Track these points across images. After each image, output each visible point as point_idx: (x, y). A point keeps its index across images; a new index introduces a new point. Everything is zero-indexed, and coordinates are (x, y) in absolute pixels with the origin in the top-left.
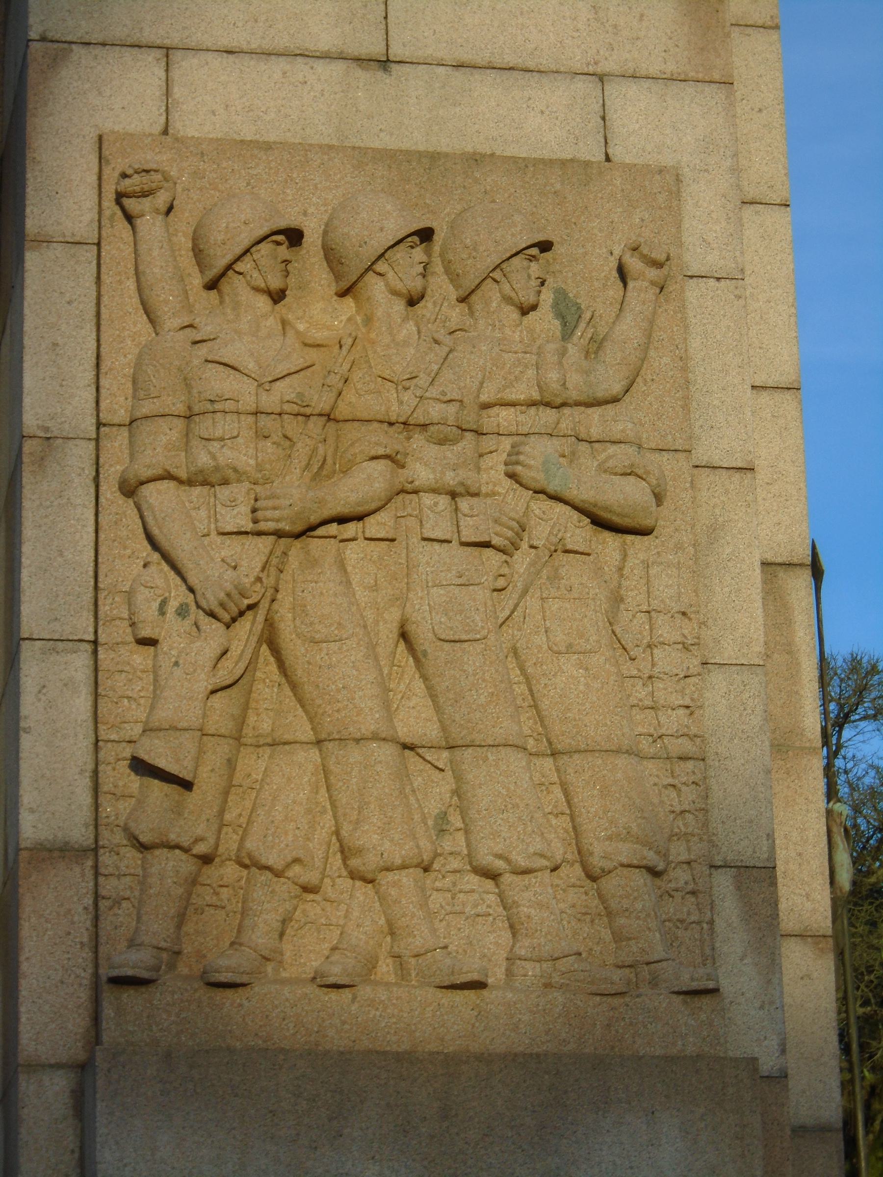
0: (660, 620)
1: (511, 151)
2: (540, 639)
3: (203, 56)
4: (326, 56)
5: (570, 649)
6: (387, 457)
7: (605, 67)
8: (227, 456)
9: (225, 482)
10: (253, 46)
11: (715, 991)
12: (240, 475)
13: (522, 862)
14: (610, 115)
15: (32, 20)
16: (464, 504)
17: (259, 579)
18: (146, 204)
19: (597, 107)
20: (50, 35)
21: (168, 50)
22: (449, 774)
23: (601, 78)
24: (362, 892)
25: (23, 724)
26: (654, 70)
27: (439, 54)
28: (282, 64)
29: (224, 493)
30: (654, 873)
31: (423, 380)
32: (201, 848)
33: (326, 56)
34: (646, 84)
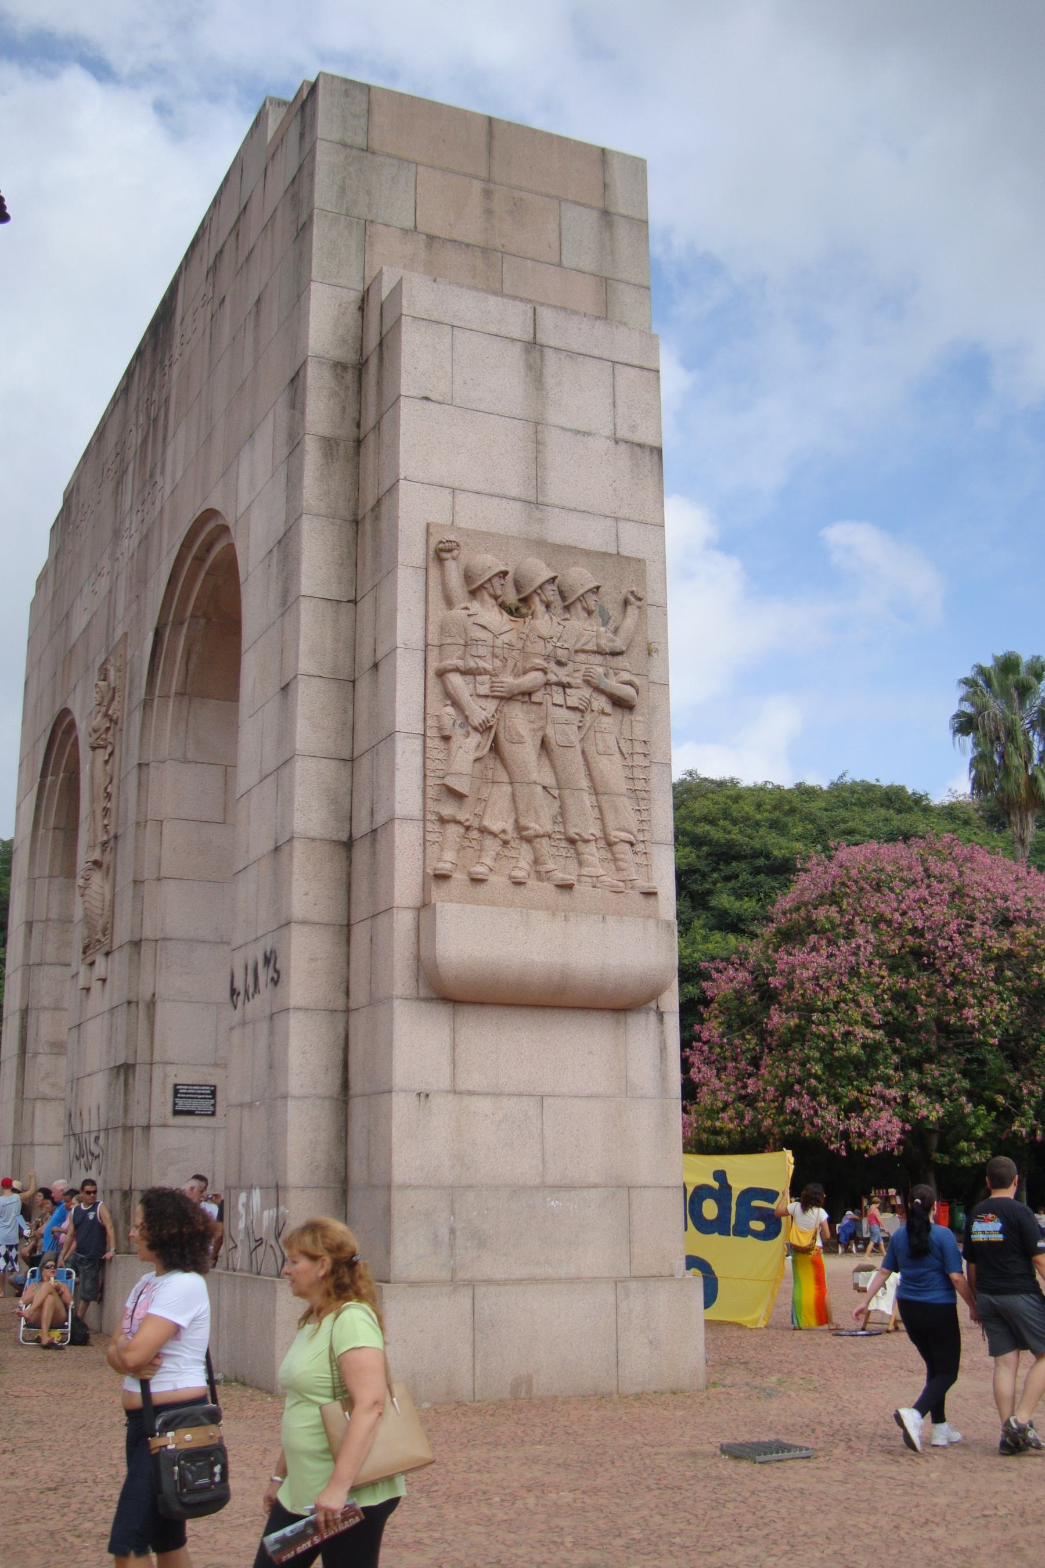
0: (636, 743)
1: (582, 546)
2: (593, 748)
3: (467, 493)
4: (513, 499)
7: (619, 515)
8: (482, 664)
9: (480, 674)
12: (486, 672)
13: (586, 837)
14: (620, 535)
15: (401, 470)
16: (568, 691)
17: (493, 716)
19: (615, 531)
20: (408, 478)
21: (454, 489)
22: (558, 800)
23: (616, 519)
24: (525, 847)
25: (397, 767)
26: (635, 518)
27: (556, 503)
28: (497, 500)
29: (479, 678)
30: (632, 844)
32: (467, 824)
33: (513, 499)
34: (633, 523)
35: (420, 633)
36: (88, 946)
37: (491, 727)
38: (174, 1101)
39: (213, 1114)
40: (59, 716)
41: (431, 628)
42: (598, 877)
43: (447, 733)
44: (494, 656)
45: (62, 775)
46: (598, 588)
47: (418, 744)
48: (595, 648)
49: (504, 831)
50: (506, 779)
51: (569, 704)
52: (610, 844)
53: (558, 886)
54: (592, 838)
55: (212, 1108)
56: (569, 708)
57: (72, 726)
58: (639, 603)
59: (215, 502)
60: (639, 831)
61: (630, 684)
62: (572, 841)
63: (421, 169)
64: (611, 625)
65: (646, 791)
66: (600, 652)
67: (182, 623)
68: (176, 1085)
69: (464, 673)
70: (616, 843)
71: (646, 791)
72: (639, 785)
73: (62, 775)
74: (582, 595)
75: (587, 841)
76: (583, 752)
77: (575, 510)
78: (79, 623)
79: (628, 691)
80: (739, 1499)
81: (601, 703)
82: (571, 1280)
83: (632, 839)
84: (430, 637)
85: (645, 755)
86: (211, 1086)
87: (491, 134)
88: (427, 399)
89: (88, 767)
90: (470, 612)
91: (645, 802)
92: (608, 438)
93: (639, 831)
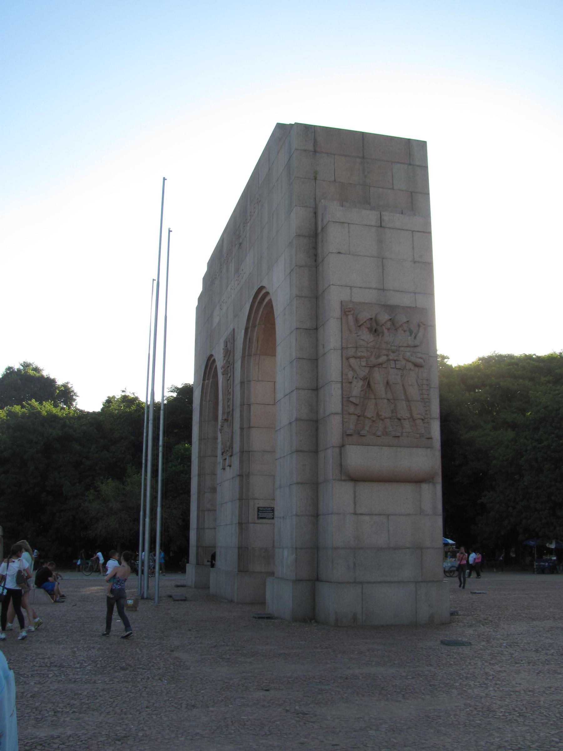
5: (411, 385)
6: (386, 355)
8: (363, 354)
9: (363, 358)
10: (341, 428)
11: (432, 438)
13: (404, 418)
16: (397, 362)
18: (350, 313)
21: (351, 287)
29: (362, 360)
30: (423, 420)
31: (391, 343)
32: (359, 415)
35: (340, 343)
36: (224, 452)
37: (367, 378)
38: (258, 513)
39: (273, 518)
40: (209, 357)
41: (343, 341)
42: (409, 433)
43: (351, 381)
44: (368, 351)
45: (211, 380)
46: (408, 321)
47: (339, 385)
48: (407, 345)
49: (373, 417)
50: (373, 397)
51: (397, 367)
52: (414, 420)
53: (393, 437)
54: (407, 418)
55: (272, 516)
56: (397, 369)
57: (214, 361)
58: (424, 326)
59: (263, 284)
60: (425, 414)
61: (420, 358)
62: (399, 419)
63: (336, 156)
64: (413, 335)
65: (428, 399)
66: (408, 346)
67: (255, 327)
68: (258, 507)
69: (355, 358)
70: (416, 419)
71: (428, 399)
72: (425, 396)
73: (211, 380)
74: (402, 325)
75: (405, 419)
76: (403, 385)
77: (399, 291)
78: (216, 320)
79: (421, 361)
80: (436, 654)
81: (410, 366)
82: (399, 582)
83: (422, 417)
84: (343, 344)
85: (427, 385)
86: (272, 508)
87: (363, 137)
88: (339, 253)
89: (221, 380)
90: (358, 335)
91: (428, 403)
92: (411, 261)
93: (425, 414)
